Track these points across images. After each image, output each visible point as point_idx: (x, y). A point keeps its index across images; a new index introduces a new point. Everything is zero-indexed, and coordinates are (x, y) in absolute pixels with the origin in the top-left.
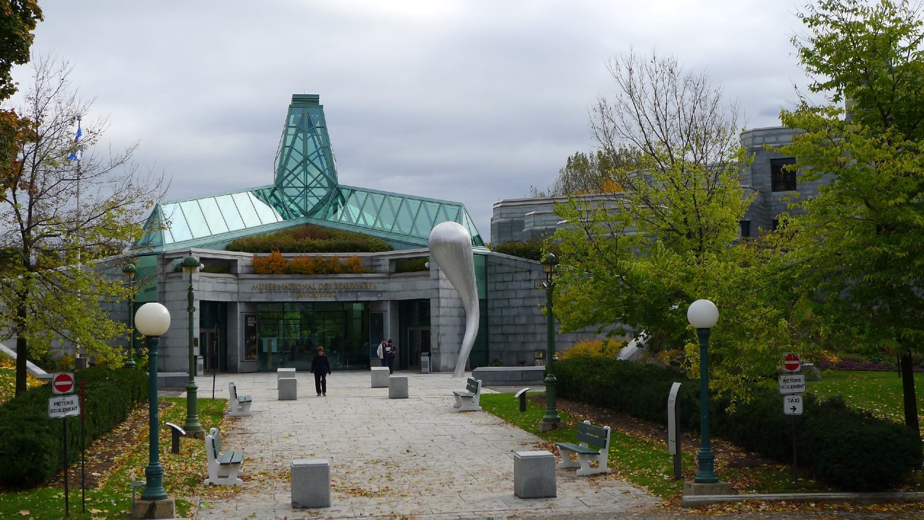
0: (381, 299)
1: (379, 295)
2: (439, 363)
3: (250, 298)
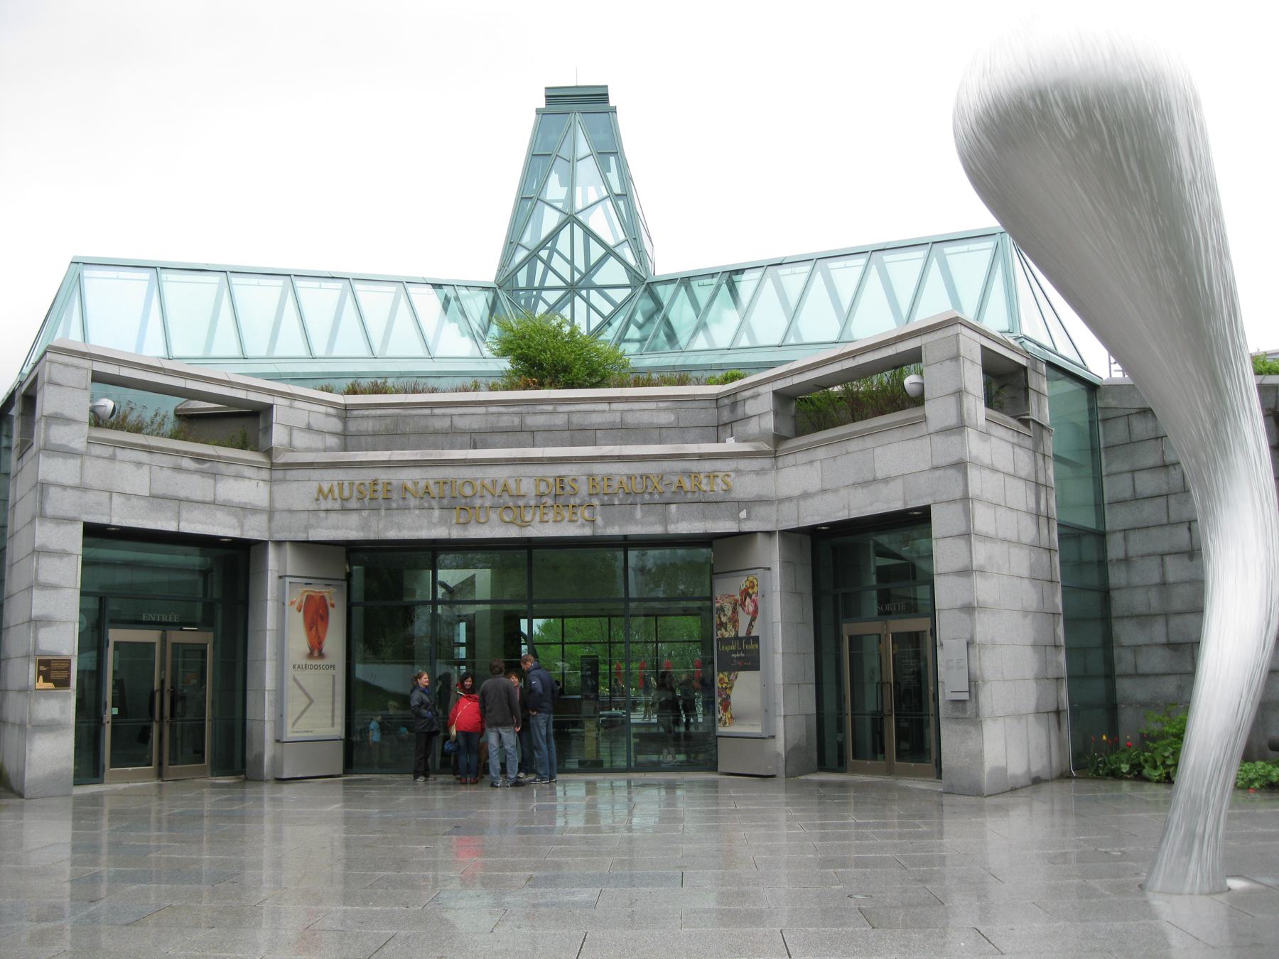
0: (747, 527)
1: (743, 514)
2: (979, 755)
3: (307, 528)
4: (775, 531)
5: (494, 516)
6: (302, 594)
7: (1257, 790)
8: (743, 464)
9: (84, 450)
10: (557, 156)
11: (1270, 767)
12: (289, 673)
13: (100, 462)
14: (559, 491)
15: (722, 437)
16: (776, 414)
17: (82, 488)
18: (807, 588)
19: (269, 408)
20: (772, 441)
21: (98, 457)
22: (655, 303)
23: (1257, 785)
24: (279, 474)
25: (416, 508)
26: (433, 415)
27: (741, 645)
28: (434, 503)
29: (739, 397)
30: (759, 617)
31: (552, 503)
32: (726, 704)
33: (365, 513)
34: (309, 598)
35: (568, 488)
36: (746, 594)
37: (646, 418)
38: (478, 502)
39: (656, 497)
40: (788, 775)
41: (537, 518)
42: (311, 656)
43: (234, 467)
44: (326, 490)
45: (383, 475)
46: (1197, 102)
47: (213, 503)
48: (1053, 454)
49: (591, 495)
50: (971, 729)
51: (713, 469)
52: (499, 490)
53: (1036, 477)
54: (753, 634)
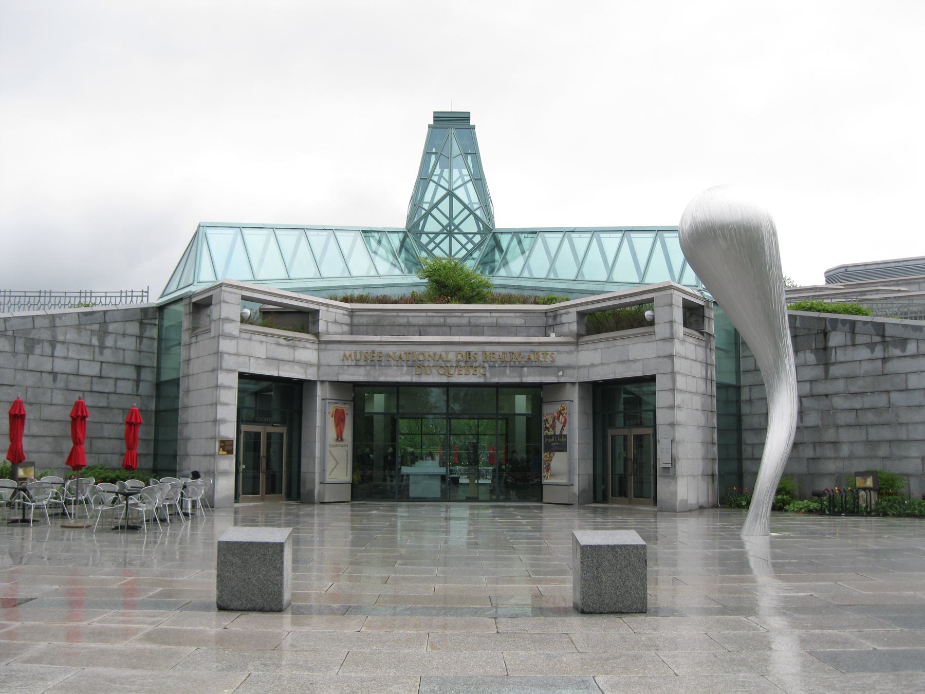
0: (562, 380)
1: (560, 373)
2: (675, 493)
3: (337, 375)
4: (576, 382)
5: (434, 371)
6: (334, 408)
7: (803, 513)
8: (561, 348)
9: (238, 335)
10: (441, 154)
11: (810, 503)
12: (328, 448)
13: (245, 341)
14: (468, 359)
15: (548, 332)
16: (578, 323)
17: (237, 355)
18: (590, 411)
19: (317, 312)
20: (575, 336)
21: (244, 339)
22: (496, 242)
23: (803, 510)
24: (323, 346)
25: (394, 366)
26: (398, 316)
27: (557, 438)
28: (404, 364)
29: (558, 313)
30: (567, 425)
31: (464, 365)
32: (548, 468)
33: (368, 368)
34: (337, 410)
35: (472, 358)
36: (560, 413)
37: (509, 321)
38: (426, 364)
39: (517, 363)
40: (579, 504)
41: (457, 373)
42: (337, 440)
43: (303, 342)
44: (348, 355)
45: (378, 349)
46: (775, 234)
47: (293, 362)
48: (715, 347)
49: (484, 361)
50: (672, 481)
51: (545, 350)
52: (437, 358)
53: (706, 361)
54: (564, 433)
